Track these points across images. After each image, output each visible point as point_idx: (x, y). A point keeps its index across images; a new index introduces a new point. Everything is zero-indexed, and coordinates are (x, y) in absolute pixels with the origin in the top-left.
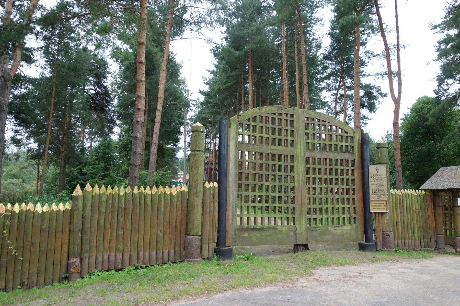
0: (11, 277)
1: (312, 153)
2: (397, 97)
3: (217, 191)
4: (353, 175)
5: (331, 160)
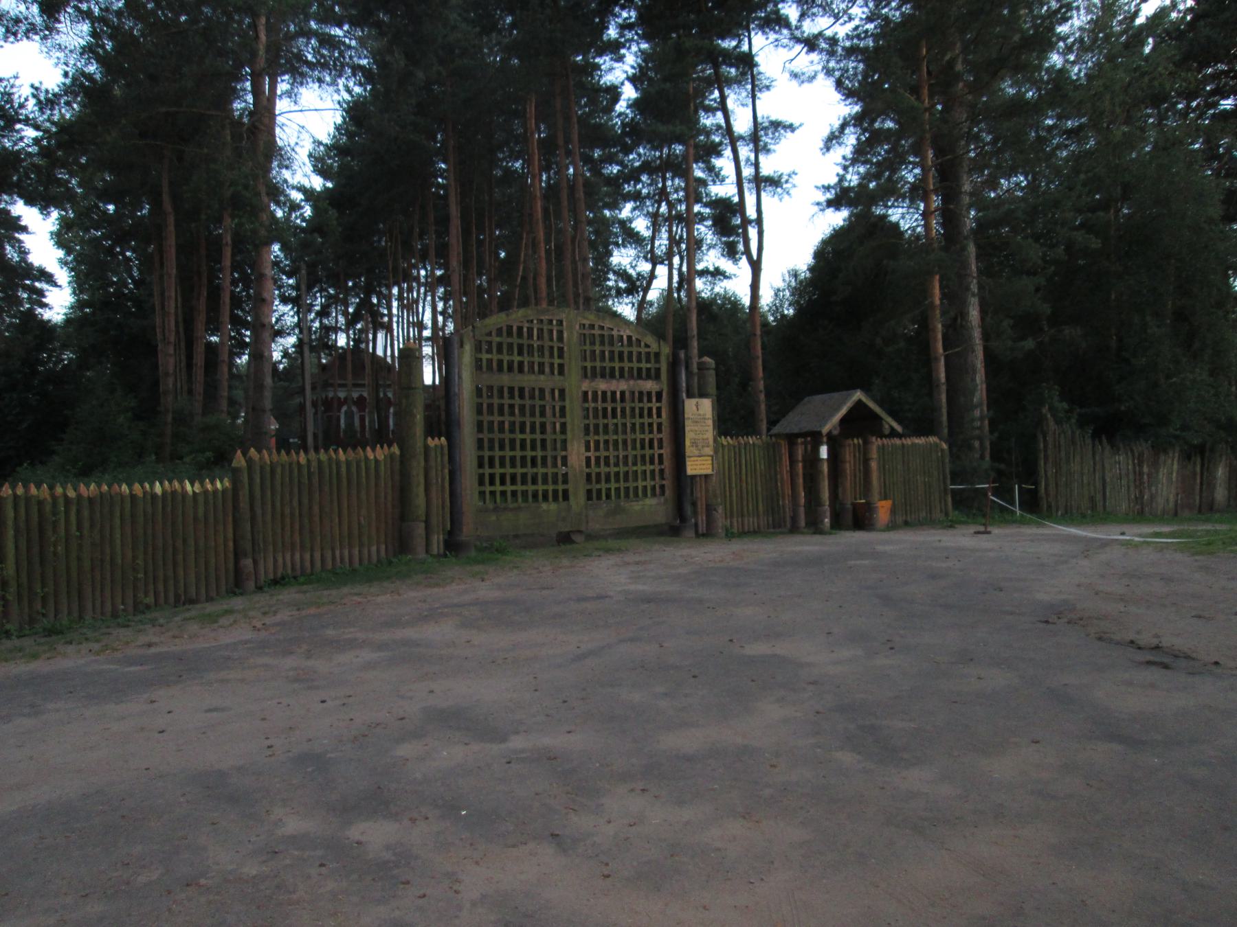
0: (161, 587)
1: (593, 384)
2: (755, 257)
3: (446, 451)
4: (659, 416)
5: (542, 372)
